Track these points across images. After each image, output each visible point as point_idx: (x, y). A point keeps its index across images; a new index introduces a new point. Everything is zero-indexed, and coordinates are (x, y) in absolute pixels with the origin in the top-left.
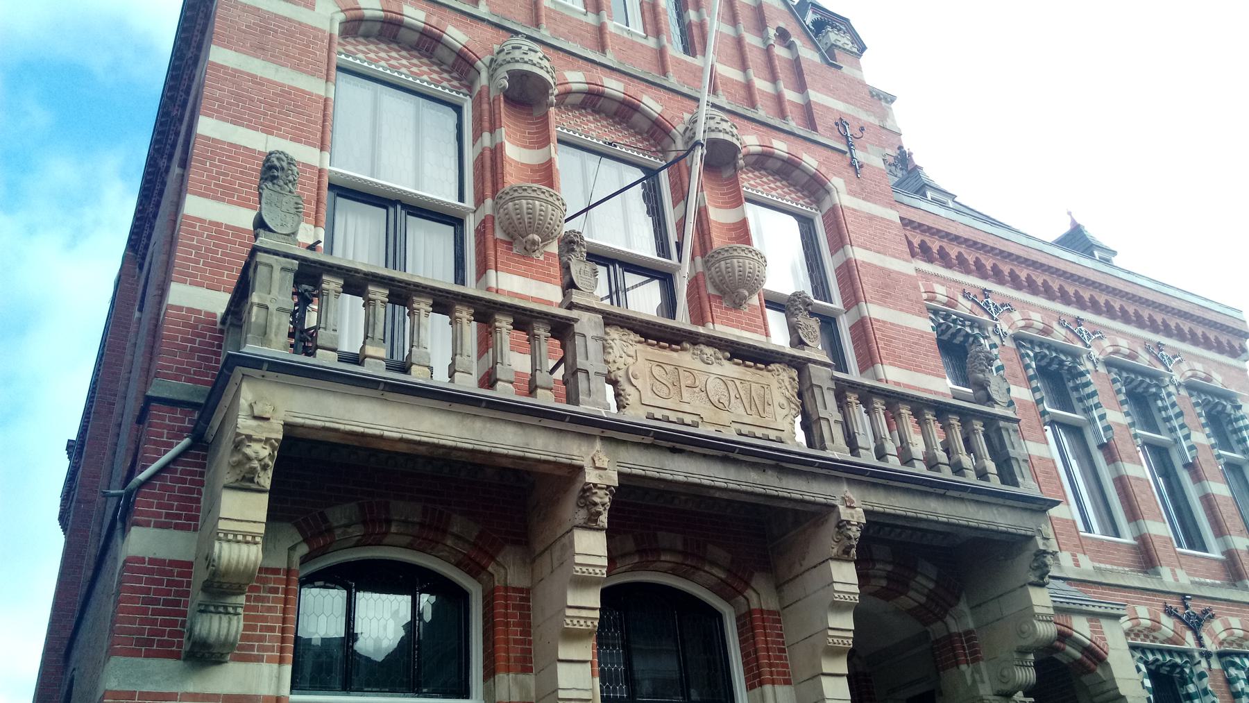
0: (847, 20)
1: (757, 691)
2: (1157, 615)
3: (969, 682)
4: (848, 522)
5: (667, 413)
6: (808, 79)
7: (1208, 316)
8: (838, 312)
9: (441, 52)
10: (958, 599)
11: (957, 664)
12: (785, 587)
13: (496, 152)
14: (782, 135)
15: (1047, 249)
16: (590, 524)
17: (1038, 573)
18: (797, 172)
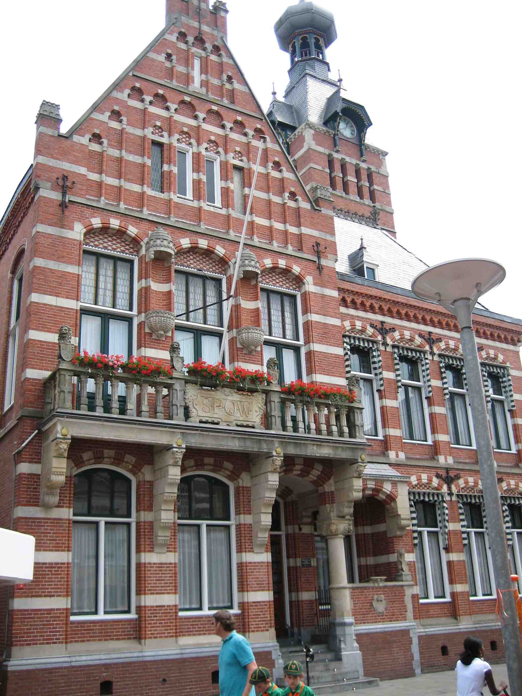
7: (503, 325)
12: (254, 478)
13: (147, 289)
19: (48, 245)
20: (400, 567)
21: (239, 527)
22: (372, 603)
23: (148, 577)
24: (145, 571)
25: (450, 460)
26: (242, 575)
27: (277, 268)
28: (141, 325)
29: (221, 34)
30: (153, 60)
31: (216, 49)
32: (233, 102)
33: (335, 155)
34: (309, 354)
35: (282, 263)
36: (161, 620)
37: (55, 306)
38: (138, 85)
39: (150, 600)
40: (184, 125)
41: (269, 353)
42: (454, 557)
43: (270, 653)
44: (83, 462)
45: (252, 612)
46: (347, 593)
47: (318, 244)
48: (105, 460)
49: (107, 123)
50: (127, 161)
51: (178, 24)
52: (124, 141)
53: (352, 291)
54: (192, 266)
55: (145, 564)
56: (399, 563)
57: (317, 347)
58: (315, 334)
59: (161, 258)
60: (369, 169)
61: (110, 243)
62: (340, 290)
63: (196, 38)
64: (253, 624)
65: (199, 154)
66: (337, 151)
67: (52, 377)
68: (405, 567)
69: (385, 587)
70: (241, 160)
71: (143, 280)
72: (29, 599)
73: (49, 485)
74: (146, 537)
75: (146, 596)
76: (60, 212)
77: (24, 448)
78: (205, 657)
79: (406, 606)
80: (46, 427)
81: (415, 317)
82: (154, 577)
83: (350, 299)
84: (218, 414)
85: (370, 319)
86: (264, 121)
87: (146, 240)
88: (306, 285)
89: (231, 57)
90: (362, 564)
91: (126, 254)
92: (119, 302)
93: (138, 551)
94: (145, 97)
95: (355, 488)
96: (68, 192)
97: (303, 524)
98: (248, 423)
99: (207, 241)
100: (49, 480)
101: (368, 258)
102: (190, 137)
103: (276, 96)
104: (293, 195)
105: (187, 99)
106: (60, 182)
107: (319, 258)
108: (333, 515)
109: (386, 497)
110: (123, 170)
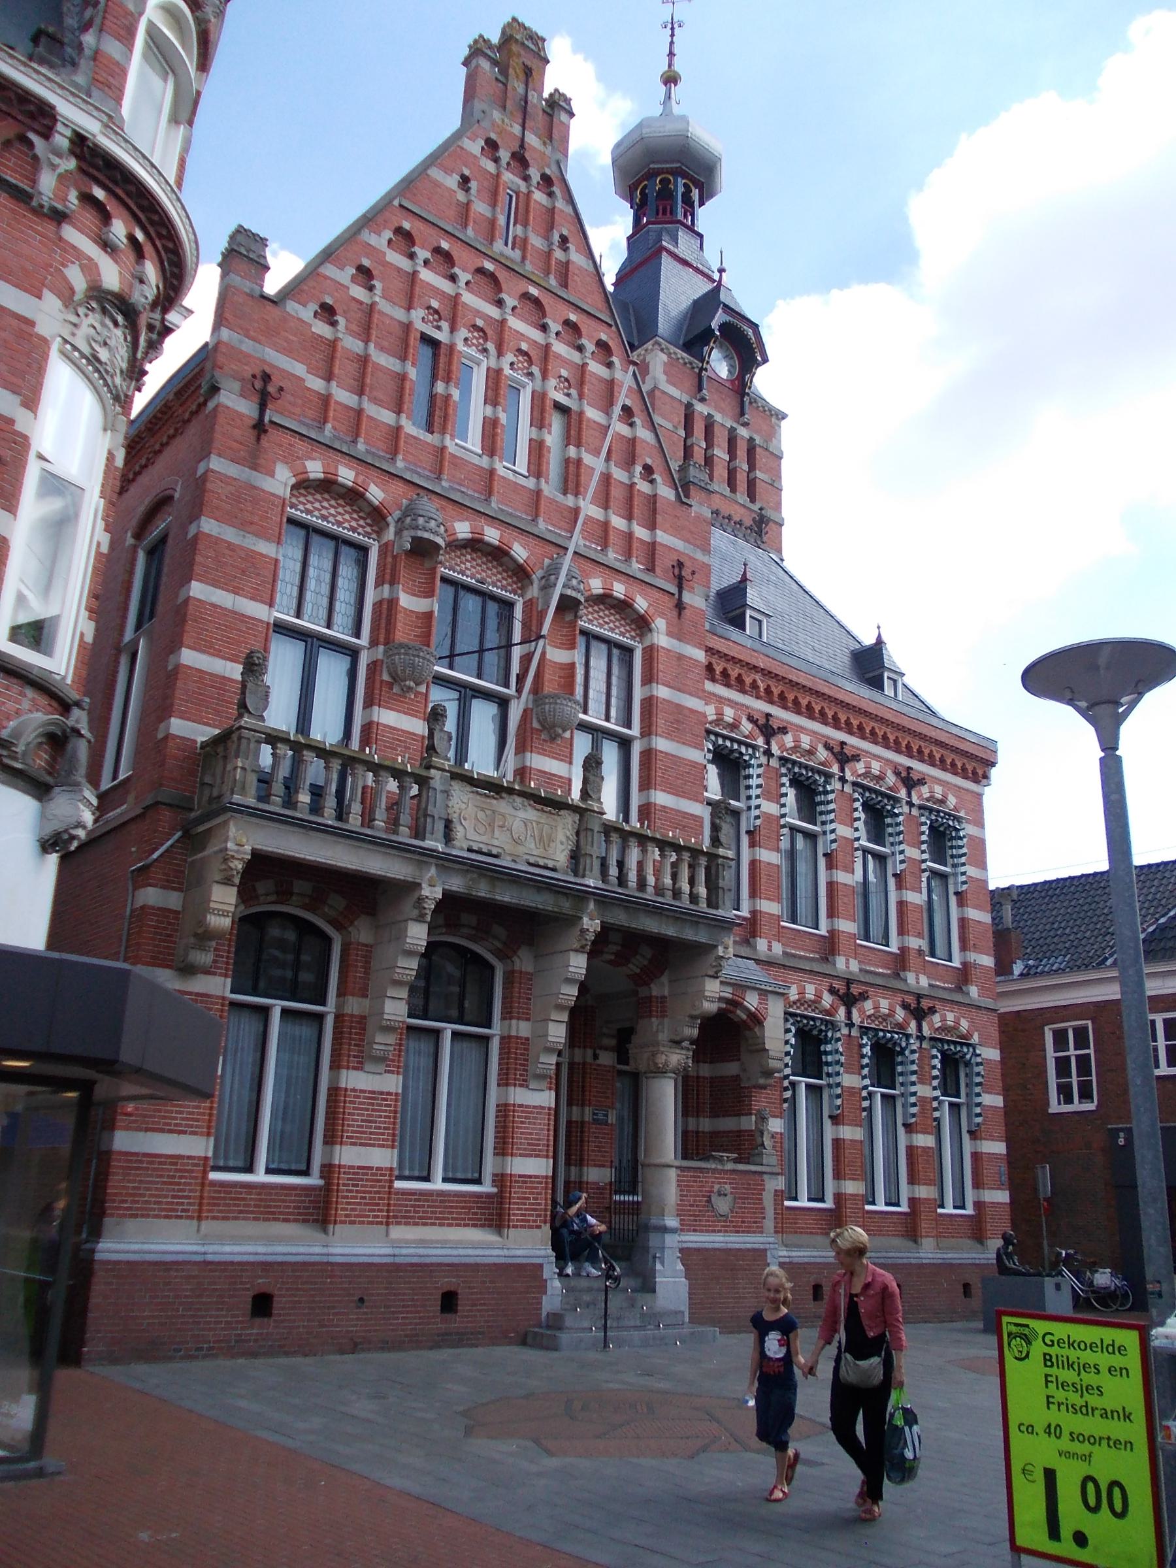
0: (757, 326)
1: (507, 1022)
3: (655, 1028)
5: (481, 846)
6: (659, 518)
7: (962, 746)
8: (635, 738)
10: (662, 973)
11: (651, 1016)
13: (392, 603)
14: (623, 578)
15: (832, 679)
16: (420, 919)
18: (629, 610)
20: (759, 1141)
21: (506, 1040)
22: (709, 1197)
23: (349, 1114)
24: (345, 1102)
25: (854, 966)
26: (505, 1127)
27: (610, 596)
28: (373, 667)
29: (560, 156)
30: (437, 184)
31: (547, 181)
32: (565, 285)
34: (648, 755)
35: (619, 590)
36: (364, 1192)
37: (230, 611)
38: (407, 225)
39: (348, 1155)
40: (478, 313)
41: (582, 745)
42: (849, 1133)
43: (540, 1266)
44: (257, 897)
45: (516, 1192)
46: (672, 1174)
47: (681, 565)
48: (294, 898)
49: (348, 288)
50: (377, 366)
51: (485, 124)
52: (374, 326)
53: (726, 655)
54: (468, 571)
55: (346, 1090)
56: (757, 1134)
57: (662, 744)
58: (660, 721)
59: (423, 550)
60: (751, 440)
61: (332, 511)
62: (709, 650)
63: (514, 155)
64: (516, 1213)
65: (499, 372)
66: (702, 400)
67: (221, 740)
68: (767, 1142)
69: (734, 1171)
70: (568, 395)
71: (386, 587)
72: (141, 1134)
73: (200, 931)
74: (353, 1043)
75: (344, 1148)
76: (252, 439)
77: (156, 860)
78: (432, 1264)
79: (763, 1208)
80: (201, 829)
81: (822, 713)
82: (358, 1115)
83: (725, 670)
84: (499, 841)
85: (747, 707)
86: (614, 328)
87: (397, 514)
89: (571, 200)
90: (690, 1128)
91: (359, 534)
92: (338, 619)
93: (335, 1066)
94: (416, 249)
96: (270, 406)
97: (600, 1048)
99: (467, 523)
100: (201, 922)
101: (753, 596)
102: (486, 339)
104: (648, 470)
105: (489, 266)
106: (258, 385)
107: (680, 588)
108: (663, 1037)
110: (368, 381)
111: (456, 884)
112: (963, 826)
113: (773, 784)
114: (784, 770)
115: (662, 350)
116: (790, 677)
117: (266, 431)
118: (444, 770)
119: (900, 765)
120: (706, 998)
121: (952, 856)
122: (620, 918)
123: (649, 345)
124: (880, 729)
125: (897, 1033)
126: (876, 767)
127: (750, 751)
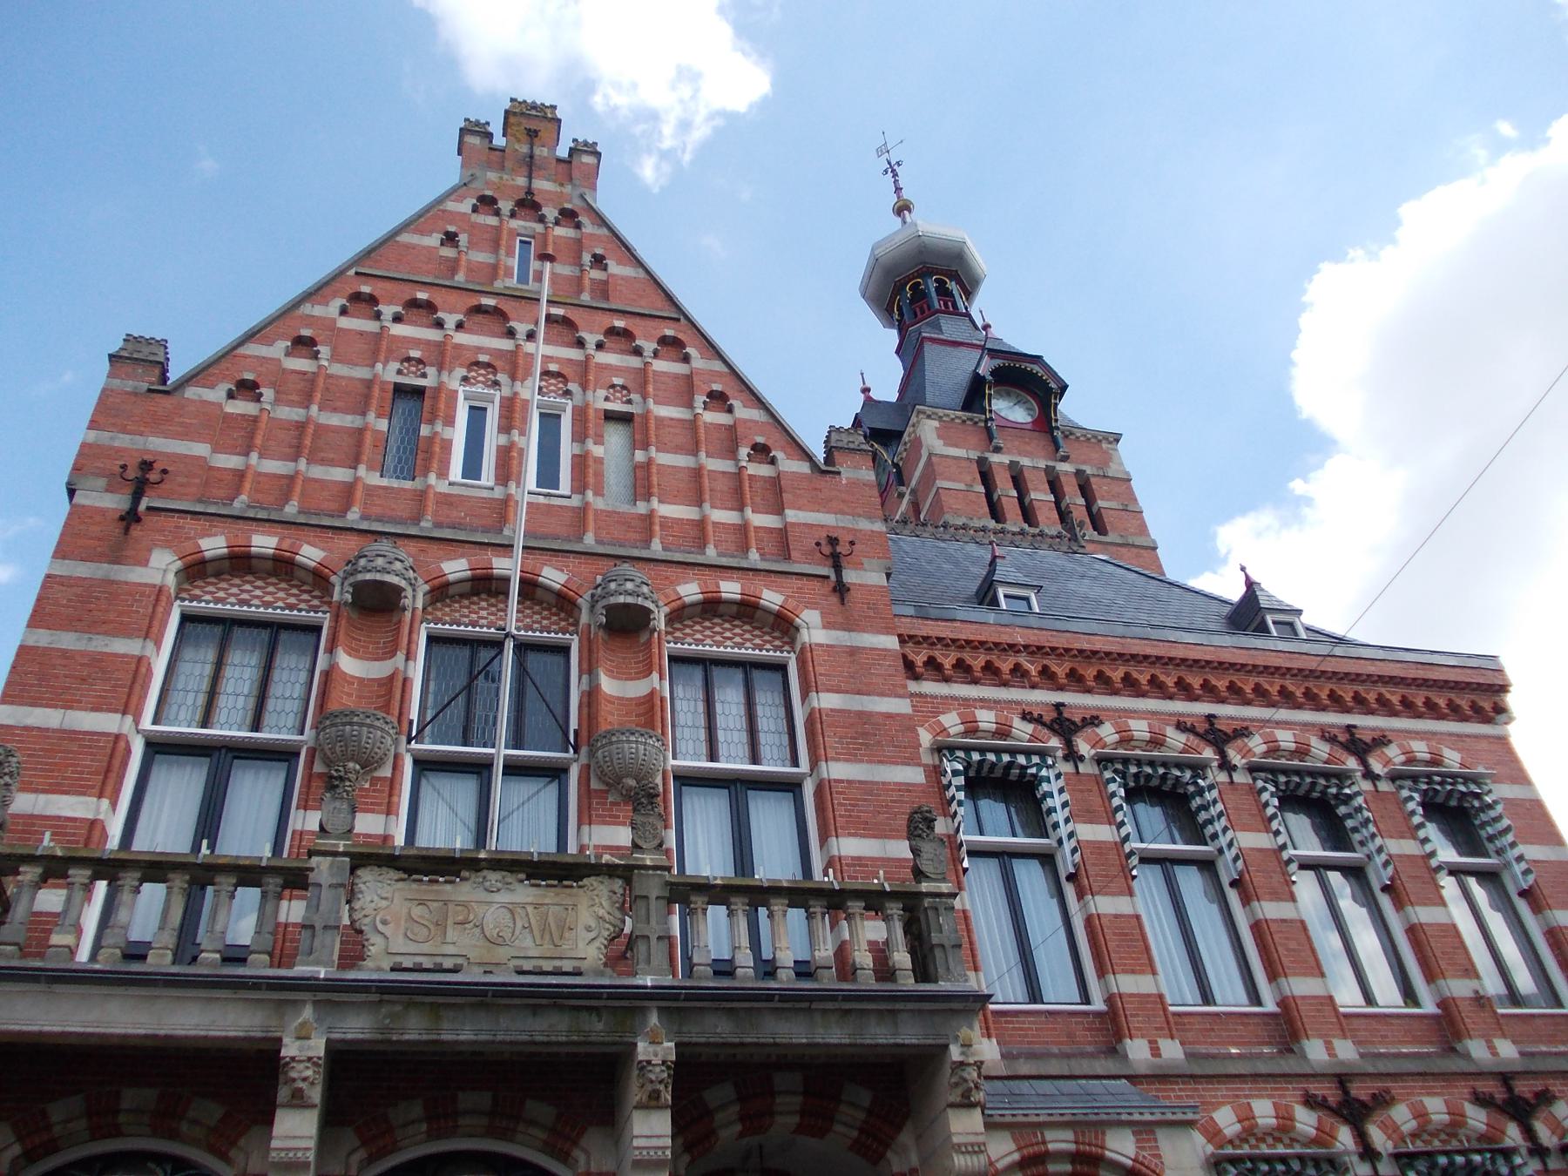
0: (1040, 357)
2: (1289, 1109)
4: (649, 1062)
5: (419, 959)
9: (300, 573)
17: (959, 1091)
19: (70, 600)
33: (995, 458)
38: (366, 289)
57: (837, 770)
58: (831, 740)
66: (997, 450)
70: (629, 402)
85: (1018, 703)
88: (804, 632)
91: (300, 610)
95: (955, 1140)
98: (558, 963)
103: (871, 394)
107: (838, 568)
109: (1073, 1162)
111: (357, 1027)
112: (1486, 788)
113: (1096, 800)
114: (1108, 775)
115: (929, 417)
116: (1077, 646)
117: (139, 520)
118: (335, 854)
119: (1332, 726)
120: (958, 1148)
121: (1491, 839)
122: (719, 1030)
123: (914, 419)
124: (1271, 684)
125: (1479, 1152)
126: (1286, 738)
127: (1036, 759)
